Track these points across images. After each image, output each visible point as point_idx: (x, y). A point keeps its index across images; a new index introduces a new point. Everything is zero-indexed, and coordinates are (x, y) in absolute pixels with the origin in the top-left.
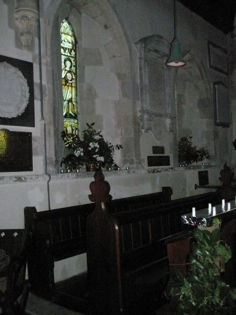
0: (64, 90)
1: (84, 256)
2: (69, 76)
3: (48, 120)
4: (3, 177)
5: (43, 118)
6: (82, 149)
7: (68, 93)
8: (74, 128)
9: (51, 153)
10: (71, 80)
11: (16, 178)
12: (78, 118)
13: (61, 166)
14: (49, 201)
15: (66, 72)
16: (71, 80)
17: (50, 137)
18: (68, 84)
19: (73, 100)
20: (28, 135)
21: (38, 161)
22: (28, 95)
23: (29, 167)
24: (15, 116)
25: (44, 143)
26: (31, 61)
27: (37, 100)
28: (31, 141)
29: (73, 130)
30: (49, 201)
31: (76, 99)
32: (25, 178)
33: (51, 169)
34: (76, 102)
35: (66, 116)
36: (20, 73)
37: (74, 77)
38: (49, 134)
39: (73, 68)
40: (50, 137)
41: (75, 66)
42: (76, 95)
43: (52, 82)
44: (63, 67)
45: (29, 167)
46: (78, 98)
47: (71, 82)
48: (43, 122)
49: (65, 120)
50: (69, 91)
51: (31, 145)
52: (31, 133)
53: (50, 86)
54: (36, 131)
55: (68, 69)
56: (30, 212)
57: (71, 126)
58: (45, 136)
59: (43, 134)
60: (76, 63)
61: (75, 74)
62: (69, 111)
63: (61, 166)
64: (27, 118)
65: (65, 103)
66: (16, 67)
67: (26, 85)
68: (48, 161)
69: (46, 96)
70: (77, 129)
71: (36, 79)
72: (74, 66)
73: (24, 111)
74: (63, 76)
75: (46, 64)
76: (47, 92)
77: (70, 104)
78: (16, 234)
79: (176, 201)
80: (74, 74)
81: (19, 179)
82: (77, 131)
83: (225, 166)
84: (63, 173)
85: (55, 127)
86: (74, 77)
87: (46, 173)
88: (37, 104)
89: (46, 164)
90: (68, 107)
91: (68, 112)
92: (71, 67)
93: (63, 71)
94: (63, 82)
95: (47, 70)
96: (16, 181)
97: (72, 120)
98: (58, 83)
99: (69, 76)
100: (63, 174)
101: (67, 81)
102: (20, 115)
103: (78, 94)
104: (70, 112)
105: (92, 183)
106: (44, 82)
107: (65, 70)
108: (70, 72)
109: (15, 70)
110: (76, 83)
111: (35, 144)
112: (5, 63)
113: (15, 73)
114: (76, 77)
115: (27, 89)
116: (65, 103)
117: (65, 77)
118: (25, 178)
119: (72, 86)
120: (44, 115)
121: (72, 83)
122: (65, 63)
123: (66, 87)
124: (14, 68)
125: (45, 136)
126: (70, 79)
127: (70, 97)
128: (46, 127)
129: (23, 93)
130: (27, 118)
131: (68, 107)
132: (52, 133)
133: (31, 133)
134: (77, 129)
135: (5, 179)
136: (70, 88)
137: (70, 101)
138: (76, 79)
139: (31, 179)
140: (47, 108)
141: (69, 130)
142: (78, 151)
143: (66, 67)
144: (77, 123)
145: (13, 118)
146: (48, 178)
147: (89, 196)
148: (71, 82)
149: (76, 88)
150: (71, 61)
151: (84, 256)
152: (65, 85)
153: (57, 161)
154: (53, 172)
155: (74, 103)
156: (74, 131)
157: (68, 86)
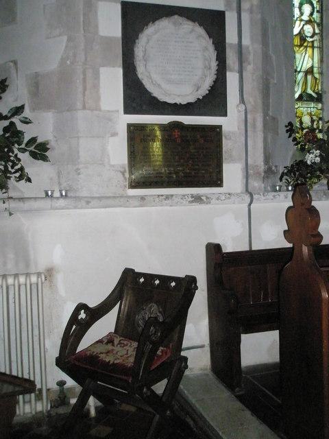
0: (297, 56)
1: (274, 336)
2: (308, 30)
3: (253, 103)
4: (172, 196)
5: (242, 101)
6: (318, 151)
7: (305, 59)
8: (315, 118)
9: (257, 158)
10: (312, 37)
11: (192, 197)
12: (324, 100)
13: (281, 180)
14: (250, 237)
15: (303, 23)
16: (312, 37)
17: (254, 132)
18: (305, 44)
19: (315, 70)
20: (216, 131)
21: (232, 172)
22: (214, 64)
23: (217, 181)
24: (192, 99)
25: (244, 142)
26: (221, 8)
27: (231, 71)
28: (220, 141)
29: (312, 121)
30: (250, 237)
31: (321, 67)
32: (207, 198)
33: (256, 184)
34: (321, 73)
35: (300, 98)
36: (200, 31)
37: (317, 31)
38: (254, 126)
39: (316, 15)
40: (254, 132)
41: (321, 12)
42: (321, 61)
43: (260, 38)
44: (296, 16)
45: (217, 181)
46: (325, 66)
47: (311, 40)
48: (242, 107)
49: (299, 104)
50: (307, 55)
51: (219, 146)
52: (220, 127)
53: (258, 47)
54: (229, 123)
55: (305, 17)
56: (214, 250)
57: (310, 114)
58: (246, 131)
59: (243, 127)
60: (322, 6)
61: (320, 25)
62: (306, 89)
63: (281, 180)
64: (214, 100)
65: (300, 76)
66: (194, 21)
67: (211, 48)
68: (251, 172)
69: (249, 64)
70: (320, 119)
71: (231, 37)
72: (318, 11)
73: (208, 92)
74: (296, 31)
75: (251, 11)
76: (251, 58)
77: (309, 77)
78: (173, 284)
79: (323, 245)
80: (318, 25)
81: (197, 199)
82: (320, 122)
83: (6, 79)
84: (280, 190)
85: (265, 114)
86: (317, 31)
87: (247, 190)
88: (232, 79)
89: (247, 177)
90: (306, 82)
91: (304, 91)
92: (312, 14)
93: (298, 22)
94: (297, 41)
95: (251, 20)
96: (192, 202)
97: (313, 105)
98: (286, 45)
99: (308, 30)
100: (275, 194)
101: (303, 38)
102: (201, 98)
103: (325, 59)
104: (309, 91)
105: (289, 208)
106: (246, 41)
107: (301, 20)
108: (309, 22)
109: (191, 27)
110: (321, 40)
111: (227, 145)
112: (176, 17)
113: (193, 31)
114: (321, 31)
115: (212, 54)
116: (300, 76)
117: (300, 33)
118: (207, 198)
119: (313, 47)
120: (245, 96)
121: (313, 42)
122: (300, 8)
123: (302, 48)
124: (190, 23)
125: (246, 131)
126: (309, 35)
127: (309, 65)
128: (249, 116)
129: (207, 62)
130: (214, 100)
131: (306, 82)
132: (260, 124)
133: (220, 127)
134: (320, 119)
135: (174, 197)
136: (310, 50)
137: (310, 71)
138: (321, 34)
139: (218, 199)
140: (251, 85)
141: (306, 120)
142: (311, 156)
143: (302, 14)
144: (322, 109)
145: (189, 104)
146: (248, 199)
147: (285, 232)
148: (311, 40)
149: (321, 48)
150: (312, 4)
151: (274, 336)
152: (301, 46)
153: (269, 172)
154: (259, 188)
155: (317, 76)
156: (315, 123)
157: (306, 47)
